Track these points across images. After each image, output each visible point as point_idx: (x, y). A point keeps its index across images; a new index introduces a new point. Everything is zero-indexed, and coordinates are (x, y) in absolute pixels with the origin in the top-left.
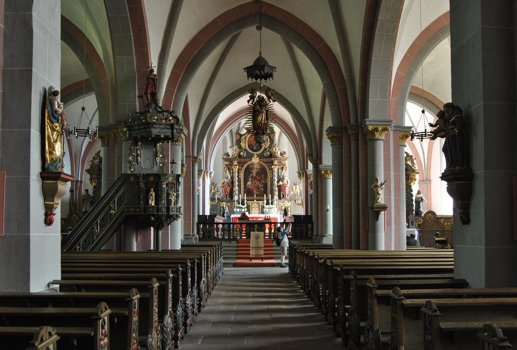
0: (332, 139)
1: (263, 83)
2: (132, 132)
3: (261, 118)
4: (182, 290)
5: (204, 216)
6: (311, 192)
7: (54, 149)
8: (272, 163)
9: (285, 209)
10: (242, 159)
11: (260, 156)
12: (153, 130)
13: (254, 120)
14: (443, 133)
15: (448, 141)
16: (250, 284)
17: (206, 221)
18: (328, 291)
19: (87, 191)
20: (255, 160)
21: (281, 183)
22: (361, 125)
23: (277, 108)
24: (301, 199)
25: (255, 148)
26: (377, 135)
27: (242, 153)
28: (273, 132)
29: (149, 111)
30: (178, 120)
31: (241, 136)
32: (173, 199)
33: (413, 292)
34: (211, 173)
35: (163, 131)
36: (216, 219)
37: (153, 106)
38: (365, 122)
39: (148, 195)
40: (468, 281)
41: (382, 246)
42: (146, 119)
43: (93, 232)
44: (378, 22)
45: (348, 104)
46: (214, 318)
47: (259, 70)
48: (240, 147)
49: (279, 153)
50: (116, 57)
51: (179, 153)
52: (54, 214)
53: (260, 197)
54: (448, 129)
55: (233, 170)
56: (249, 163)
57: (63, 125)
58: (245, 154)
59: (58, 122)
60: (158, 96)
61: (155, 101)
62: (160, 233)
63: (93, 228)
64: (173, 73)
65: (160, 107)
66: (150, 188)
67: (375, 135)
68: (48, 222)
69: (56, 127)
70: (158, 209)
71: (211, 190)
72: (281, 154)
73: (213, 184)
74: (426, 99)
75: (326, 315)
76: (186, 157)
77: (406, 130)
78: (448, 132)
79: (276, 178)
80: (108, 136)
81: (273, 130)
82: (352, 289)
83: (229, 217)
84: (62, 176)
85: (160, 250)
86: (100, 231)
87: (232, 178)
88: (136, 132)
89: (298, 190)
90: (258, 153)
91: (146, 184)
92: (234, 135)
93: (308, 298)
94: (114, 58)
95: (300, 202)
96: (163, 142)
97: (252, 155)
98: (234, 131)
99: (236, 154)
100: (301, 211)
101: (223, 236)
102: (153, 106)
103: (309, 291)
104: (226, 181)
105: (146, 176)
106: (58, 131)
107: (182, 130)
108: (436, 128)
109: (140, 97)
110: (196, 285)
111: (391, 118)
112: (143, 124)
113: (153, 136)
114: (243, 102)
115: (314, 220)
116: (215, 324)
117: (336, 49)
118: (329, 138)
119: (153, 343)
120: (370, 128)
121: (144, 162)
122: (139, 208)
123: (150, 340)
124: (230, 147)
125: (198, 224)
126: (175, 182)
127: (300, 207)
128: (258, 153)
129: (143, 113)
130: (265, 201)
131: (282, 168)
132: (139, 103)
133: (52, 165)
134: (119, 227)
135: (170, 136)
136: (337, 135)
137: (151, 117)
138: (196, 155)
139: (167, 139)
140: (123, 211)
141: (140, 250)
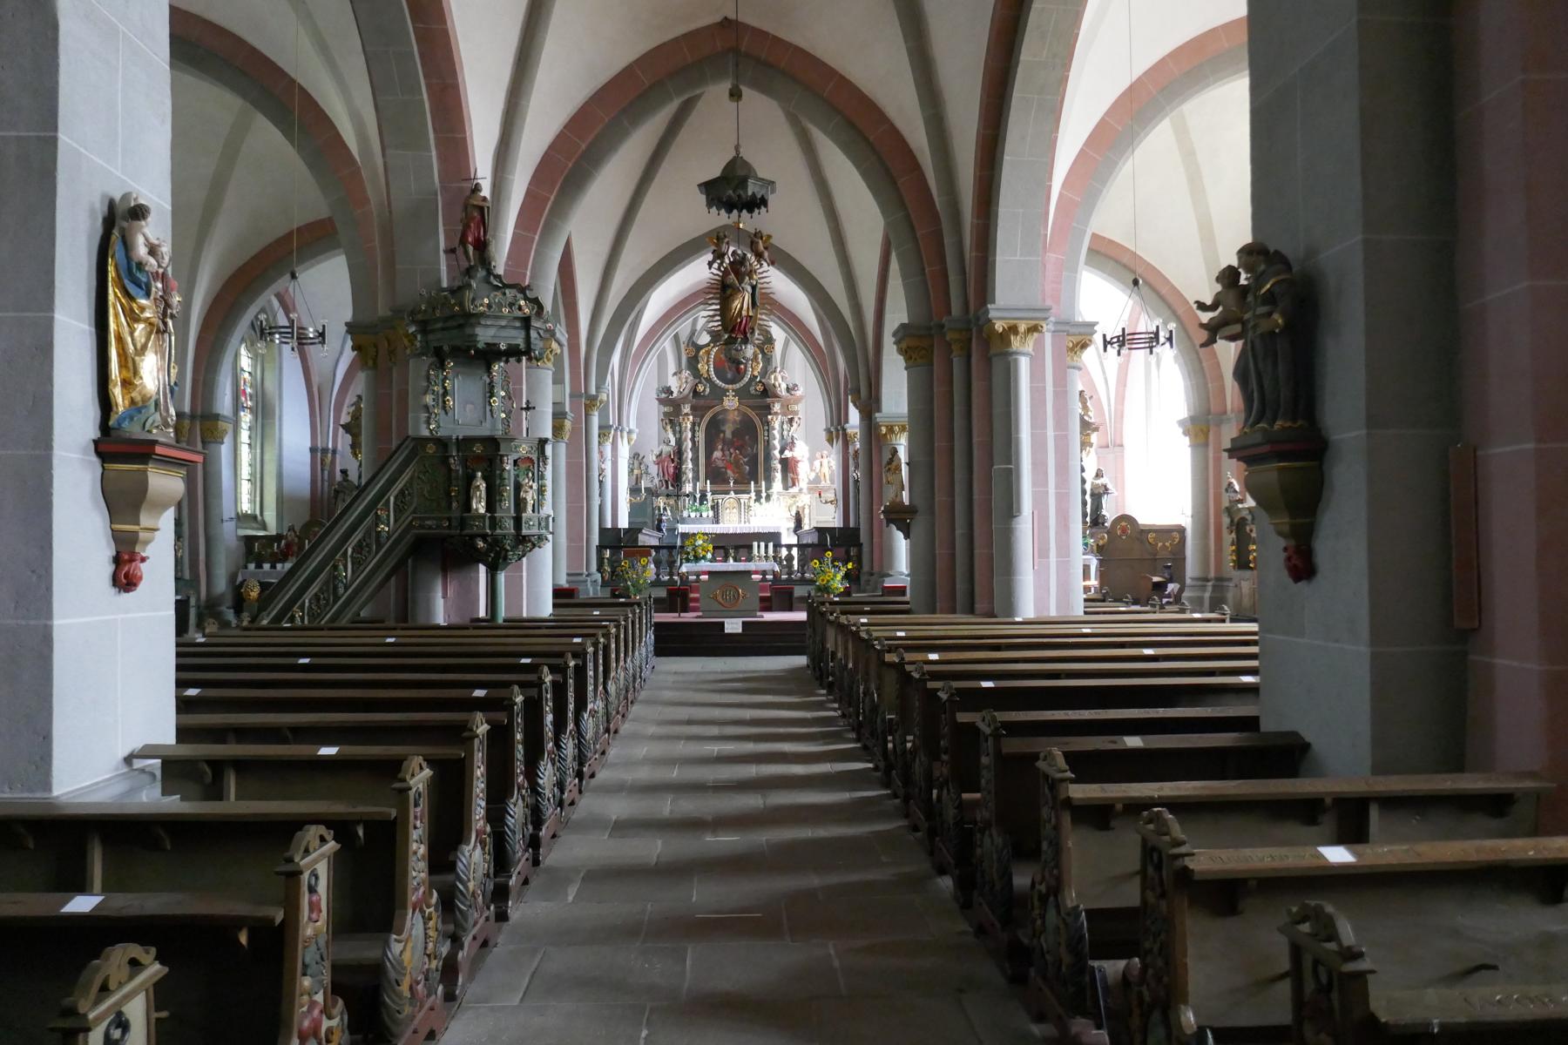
0: (906, 352)
1: (747, 222)
2: (431, 337)
3: (742, 303)
4: (526, 755)
5: (616, 530)
6: (855, 474)
7: (136, 372)
8: (768, 409)
9: (798, 513)
10: (702, 402)
11: (742, 394)
12: (479, 331)
13: (724, 310)
14: (1237, 328)
15: (1253, 348)
16: (717, 698)
17: (618, 543)
18: (910, 738)
19: (344, 472)
20: (731, 402)
21: (788, 454)
22: (978, 319)
23: (777, 282)
24: (832, 487)
25: (729, 376)
26: (1016, 342)
27: (700, 388)
28: (769, 340)
29: (470, 286)
30: (541, 307)
31: (699, 348)
32: (530, 496)
33: (1176, 793)
34: (630, 432)
35: (504, 333)
37: (481, 273)
38: (987, 311)
39: (468, 492)
40: (1308, 739)
41: (1028, 606)
42: (461, 304)
43: (335, 578)
44: (1020, 69)
45: (945, 270)
46: (618, 808)
47: (732, 190)
48: (696, 373)
49: (784, 386)
50: (388, 152)
51: (544, 389)
52: (143, 560)
53: (742, 485)
54: (1255, 316)
56: (717, 409)
57: (168, 305)
59: (148, 295)
60: (492, 248)
61: (484, 259)
62: (502, 577)
63: (335, 567)
64: (530, 195)
65: (498, 277)
66: (474, 472)
67: (1009, 344)
68: (124, 580)
69: (143, 309)
70: (494, 523)
71: (631, 471)
72: (788, 389)
73: (636, 457)
74: (1116, 261)
75: (906, 799)
76: (571, 396)
77: (1082, 330)
78: (1255, 327)
79: (777, 443)
80: (376, 346)
81: (768, 332)
82: (985, 760)
83: (672, 530)
84: (158, 450)
85: (500, 621)
87: (679, 442)
88: (439, 335)
89: (826, 470)
90: (738, 386)
91: (464, 462)
93: (858, 740)
94: (384, 155)
95: (831, 496)
96: (507, 362)
98: (684, 338)
99: (687, 388)
100: (831, 517)
101: (658, 575)
102: (481, 273)
103: (860, 725)
104: (666, 449)
105: (467, 442)
106: (147, 320)
107: (552, 333)
108: (1216, 313)
109: (450, 251)
110: (571, 726)
111: (1048, 303)
112: (453, 317)
113: (480, 346)
114: (698, 272)
115: (863, 538)
116: (622, 827)
117: (918, 137)
118: (900, 351)
119: (407, 956)
120: (999, 326)
121: (460, 406)
122: (449, 519)
123: (396, 948)
125: (600, 548)
126: (534, 457)
127: (831, 507)
128: (738, 386)
129: (457, 291)
130: (753, 495)
131: (791, 421)
132: (448, 266)
133: (132, 419)
134: (401, 563)
135: (522, 346)
136: (916, 344)
137: (474, 300)
139: (514, 353)
141: (455, 620)
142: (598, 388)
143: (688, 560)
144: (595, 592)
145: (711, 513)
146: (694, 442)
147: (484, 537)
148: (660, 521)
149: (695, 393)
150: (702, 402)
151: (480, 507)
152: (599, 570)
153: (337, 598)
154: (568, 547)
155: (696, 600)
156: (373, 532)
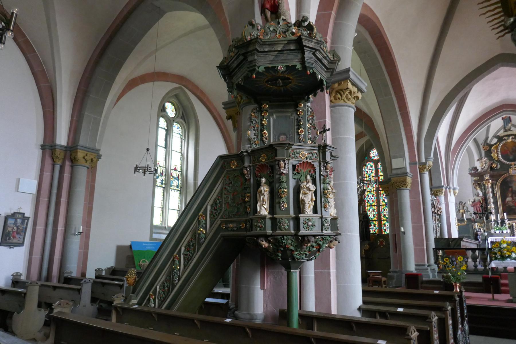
17: (447, 247)
27: (494, 165)
32: (308, 199)
34: (454, 189)
36: (462, 243)
48: (491, 158)
55: (484, 185)
58: (499, 166)
63: (174, 261)
73: (460, 204)
76: (410, 164)
86: (184, 267)
87: (485, 194)
92: (481, 147)
97: (509, 166)
98: (481, 141)
99: (486, 166)
104: (477, 198)
124: (478, 160)
125: (436, 250)
138: (423, 160)
140: (219, 229)
142: (426, 159)
143: (496, 259)
144: (434, 276)
145: (509, 231)
146: (493, 194)
147: (266, 237)
148: (477, 235)
149: (491, 168)
150: (496, 173)
151: (264, 210)
152: (435, 263)
153: (174, 287)
154: (415, 249)
155: (506, 285)
156: (196, 235)
